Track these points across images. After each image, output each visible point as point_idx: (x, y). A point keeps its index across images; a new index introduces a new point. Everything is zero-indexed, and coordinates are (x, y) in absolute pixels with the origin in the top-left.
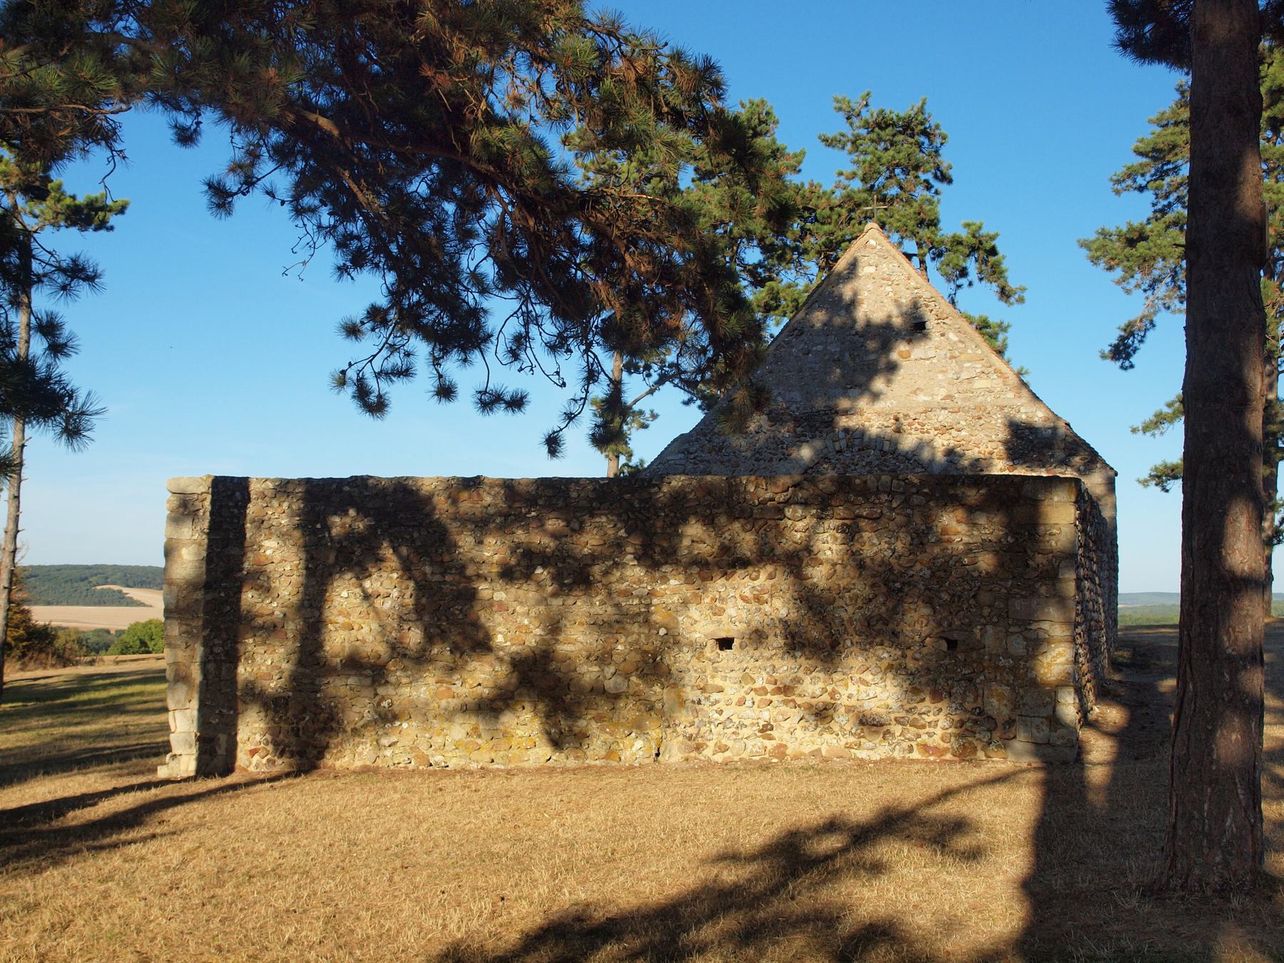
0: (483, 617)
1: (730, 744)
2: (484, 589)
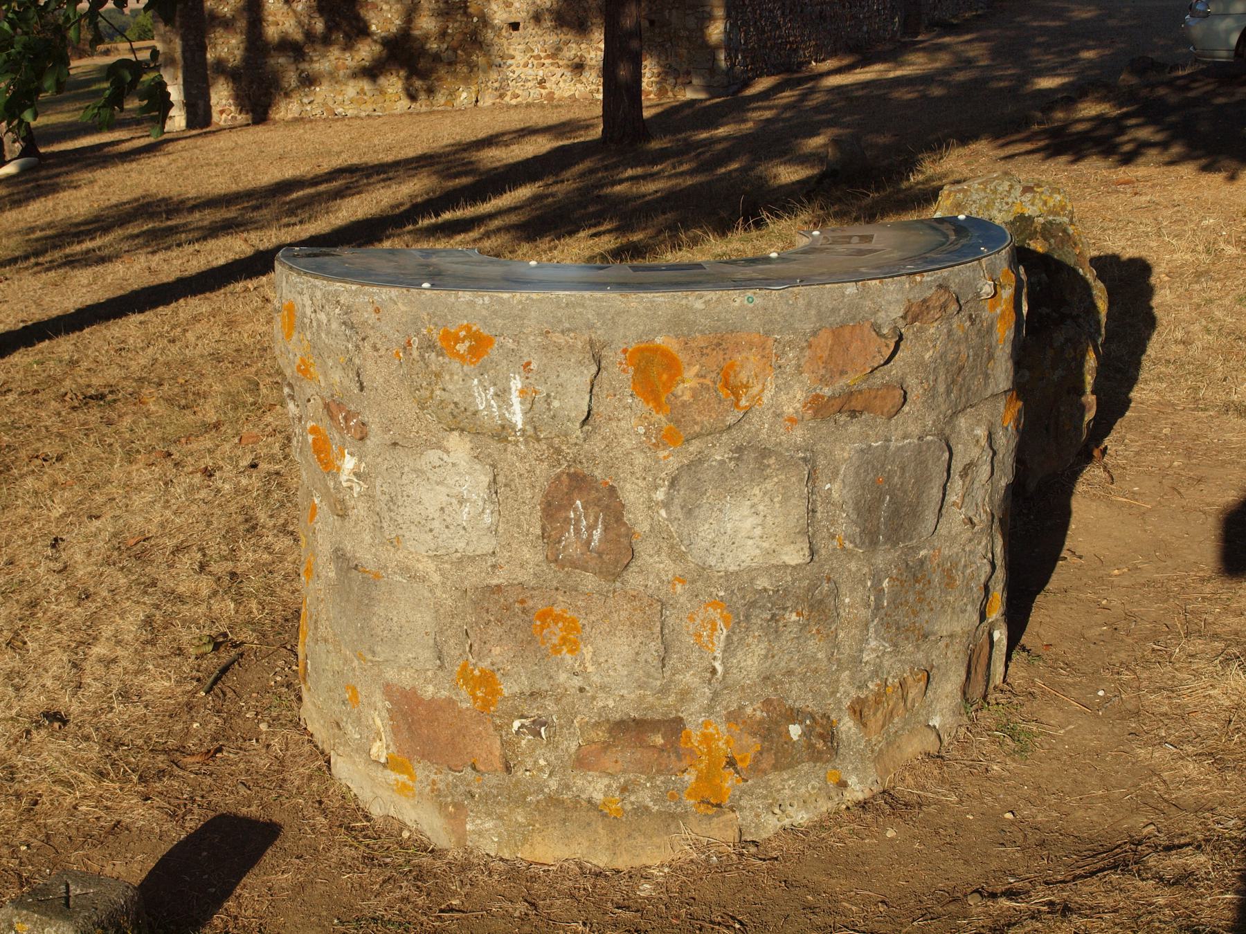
0: (362, 12)
1: (520, 92)
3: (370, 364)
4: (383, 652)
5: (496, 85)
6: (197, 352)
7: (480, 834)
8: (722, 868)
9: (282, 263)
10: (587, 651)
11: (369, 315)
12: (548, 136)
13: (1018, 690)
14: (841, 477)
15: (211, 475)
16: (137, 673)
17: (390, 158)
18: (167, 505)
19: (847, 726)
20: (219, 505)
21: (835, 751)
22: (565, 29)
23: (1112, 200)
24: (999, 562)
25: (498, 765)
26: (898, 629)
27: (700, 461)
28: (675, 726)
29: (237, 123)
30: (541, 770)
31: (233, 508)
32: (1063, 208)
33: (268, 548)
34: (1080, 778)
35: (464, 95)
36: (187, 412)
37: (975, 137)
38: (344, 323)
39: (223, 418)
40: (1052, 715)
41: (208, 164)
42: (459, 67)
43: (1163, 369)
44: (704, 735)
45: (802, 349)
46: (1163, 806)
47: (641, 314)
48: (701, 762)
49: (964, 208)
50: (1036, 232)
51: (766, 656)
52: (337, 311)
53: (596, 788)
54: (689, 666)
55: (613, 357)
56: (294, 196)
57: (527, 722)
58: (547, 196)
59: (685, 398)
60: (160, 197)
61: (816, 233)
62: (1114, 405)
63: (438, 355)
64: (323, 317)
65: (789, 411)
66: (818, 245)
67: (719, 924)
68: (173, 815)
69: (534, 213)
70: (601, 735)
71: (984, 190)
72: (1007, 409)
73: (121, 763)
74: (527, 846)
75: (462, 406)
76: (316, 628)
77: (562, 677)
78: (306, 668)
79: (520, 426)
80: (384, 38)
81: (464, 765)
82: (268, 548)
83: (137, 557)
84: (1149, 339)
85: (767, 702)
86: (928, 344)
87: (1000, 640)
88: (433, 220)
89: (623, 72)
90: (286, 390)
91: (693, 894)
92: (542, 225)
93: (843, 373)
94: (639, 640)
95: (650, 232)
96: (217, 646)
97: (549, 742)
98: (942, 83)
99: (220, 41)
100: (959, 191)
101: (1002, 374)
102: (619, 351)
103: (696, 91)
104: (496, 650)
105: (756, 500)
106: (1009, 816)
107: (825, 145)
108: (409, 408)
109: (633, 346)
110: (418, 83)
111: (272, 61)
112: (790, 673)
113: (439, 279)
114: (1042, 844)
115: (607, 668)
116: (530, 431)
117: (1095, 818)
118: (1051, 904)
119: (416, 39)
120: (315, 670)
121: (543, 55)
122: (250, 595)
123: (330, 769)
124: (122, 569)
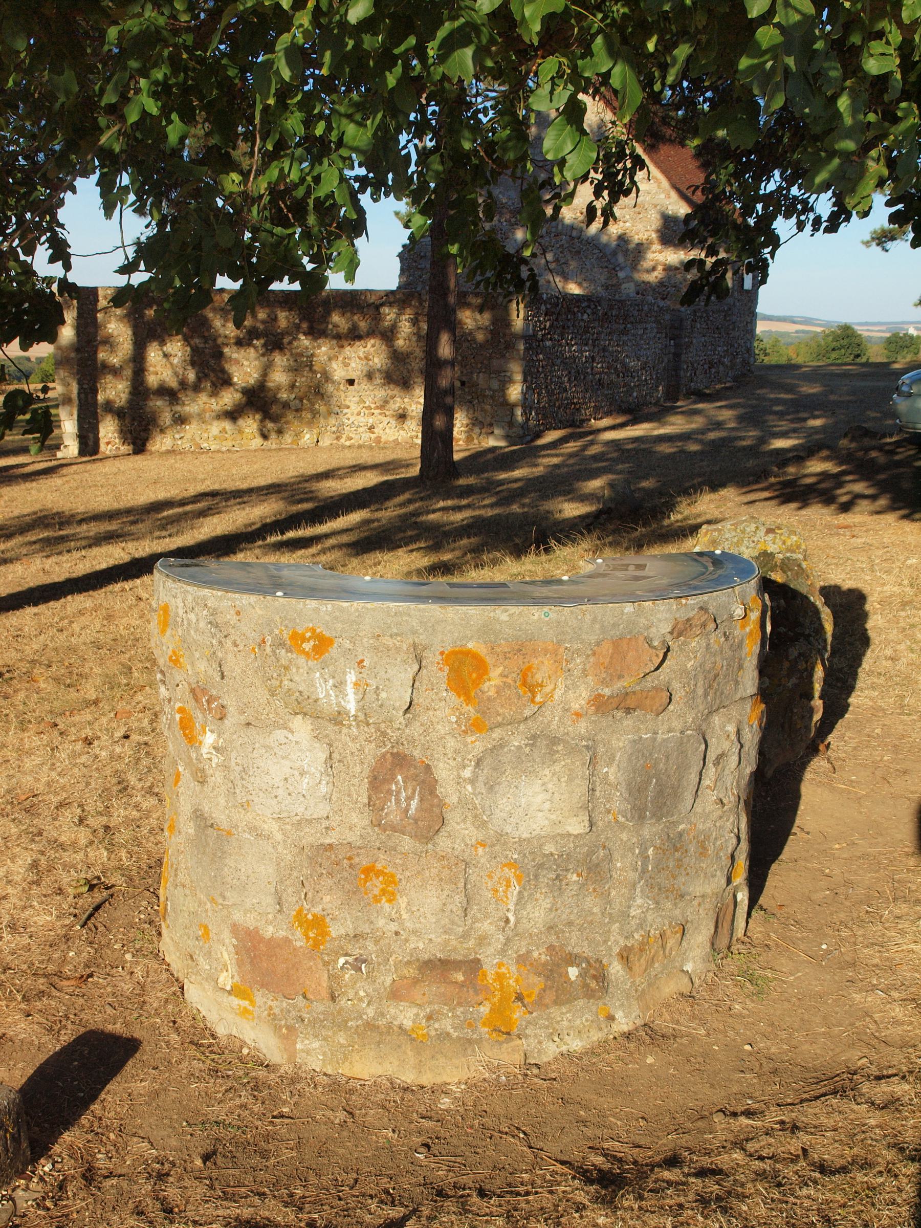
0: (227, 366)
2: (226, 350)
3: (230, 657)
4: (232, 897)
5: (334, 429)
6: (81, 640)
7: (308, 1052)
8: (510, 1087)
9: (159, 571)
10: (403, 901)
11: (231, 617)
12: (375, 472)
13: (756, 942)
14: (616, 762)
15: (90, 744)
16: (24, 908)
17: (245, 486)
18: (53, 767)
19: (616, 969)
20: (97, 769)
21: (605, 989)
22: (392, 386)
23: (834, 541)
24: (744, 836)
25: (325, 994)
26: (660, 889)
27: (502, 746)
28: (473, 966)
29: (121, 452)
30: (361, 1000)
31: (108, 771)
32: (798, 547)
33: (137, 807)
34: (806, 1017)
35: (308, 436)
36: (71, 690)
37: (723, 485)
38: (210, 623)
39: (101, 695)
40: (784, 964)
41: (96, 486)
42: (304, 413)
43: (875, 680)
44: (497, 973)
45: (588, 656)
46: (874, 1042)
47: (455, 623)
48: (494, 996)
49: (719, 544)
50: (776, 565)
51: (551, 910)
52: (205, 612)
53: (406, 1016)
54: (486, 917)
55: (432, 658)
56: (165, 514)
57: (350, 959)
58: (373, 521)
59: (490, 693)
60: (55, 511)
61: (600, 561)
62: (836, 709)
63: (287, 652)
64: (192, 617)
65: (575, 706)
66: (601, 571)
67: (506, 1133)
68: (51, 1030)
69: (362, 535)
70: (411, 972)
71: (735, 530)
72: (752, 710)
73: (7, 985)
74: (347, 1064)
75: (306, 694)
76: (176, 875)
77: (381, 922)
78: (166, 909)
79: (353, 712)
80: (243, 388)
81: (297, 994)
82: (137, 807)
83: (27, 811)
84: (864, 655)
85: (551, 948)
86: (690, 655)
87: (742, 900)
88: (279, 538)
89: (439, 422)
90: (159, 676)
91: (485, 1107)
92: (368, 543)
93: (620, 677)
94: (446, 893)
95: (458, 553)
96: (92, 888)
97: (368, 977)
98: (697, 441)
99: (109, 386)
100: (715, 530)
101: (749, 681)
102: (437, 653)
103: (497, 439)
104: (327, 899)
105: (546, 779)
106: (748, 1047)
107: (603, 488)
108: (262, 695)
109: (448, 649)
110: (270, 425)
111: (151, 404)
112: (570, 924)
113: (294, 590)
114: (775, 1072)
115: (420, 917)
116: (361, 717)
117: (818, 1051)
118: (782, 1122)
119: (270, 389)
120: (174, 910)
121: (373, 406)
122: (121, 845)
123: (183, 994)
124: (14, 820)
